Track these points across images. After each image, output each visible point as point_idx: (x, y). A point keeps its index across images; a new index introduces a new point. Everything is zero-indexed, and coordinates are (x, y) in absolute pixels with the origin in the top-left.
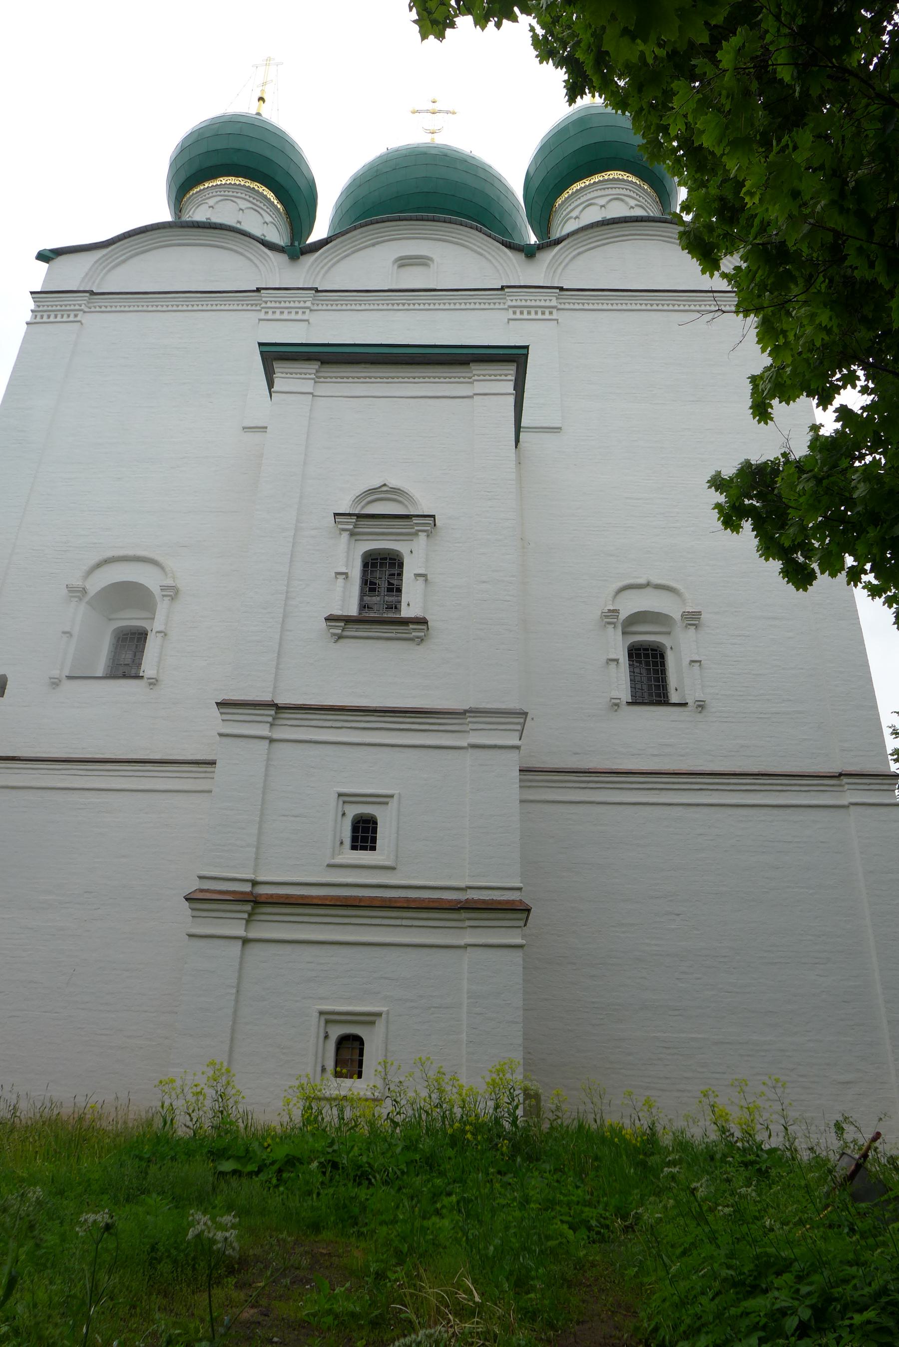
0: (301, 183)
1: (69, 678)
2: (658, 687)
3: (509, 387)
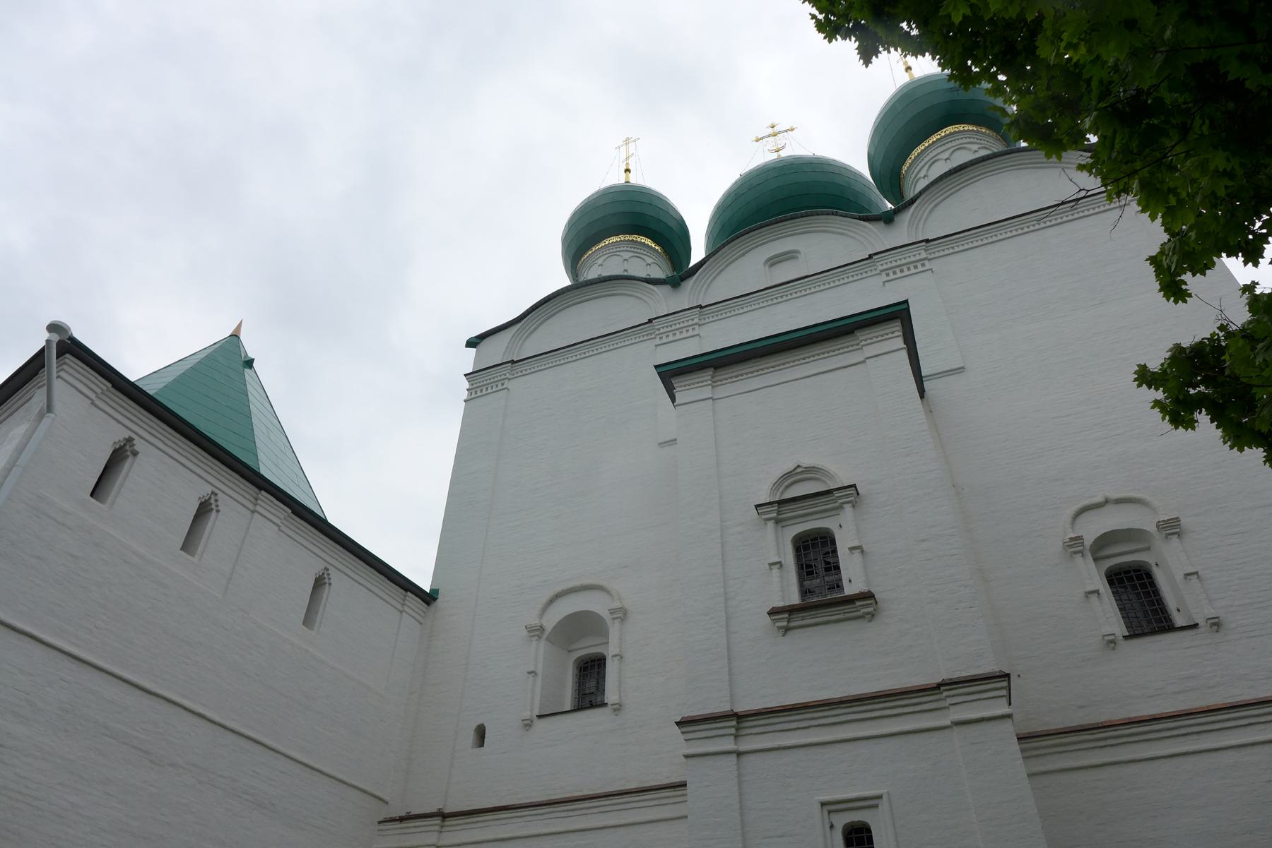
0: (672, 224)
1: (540, 717)
2: (1155, 612)
3: (900, 343)
